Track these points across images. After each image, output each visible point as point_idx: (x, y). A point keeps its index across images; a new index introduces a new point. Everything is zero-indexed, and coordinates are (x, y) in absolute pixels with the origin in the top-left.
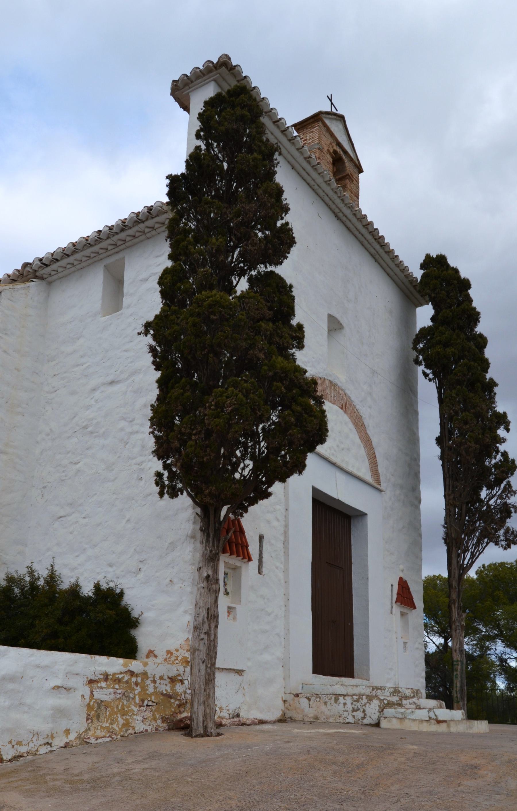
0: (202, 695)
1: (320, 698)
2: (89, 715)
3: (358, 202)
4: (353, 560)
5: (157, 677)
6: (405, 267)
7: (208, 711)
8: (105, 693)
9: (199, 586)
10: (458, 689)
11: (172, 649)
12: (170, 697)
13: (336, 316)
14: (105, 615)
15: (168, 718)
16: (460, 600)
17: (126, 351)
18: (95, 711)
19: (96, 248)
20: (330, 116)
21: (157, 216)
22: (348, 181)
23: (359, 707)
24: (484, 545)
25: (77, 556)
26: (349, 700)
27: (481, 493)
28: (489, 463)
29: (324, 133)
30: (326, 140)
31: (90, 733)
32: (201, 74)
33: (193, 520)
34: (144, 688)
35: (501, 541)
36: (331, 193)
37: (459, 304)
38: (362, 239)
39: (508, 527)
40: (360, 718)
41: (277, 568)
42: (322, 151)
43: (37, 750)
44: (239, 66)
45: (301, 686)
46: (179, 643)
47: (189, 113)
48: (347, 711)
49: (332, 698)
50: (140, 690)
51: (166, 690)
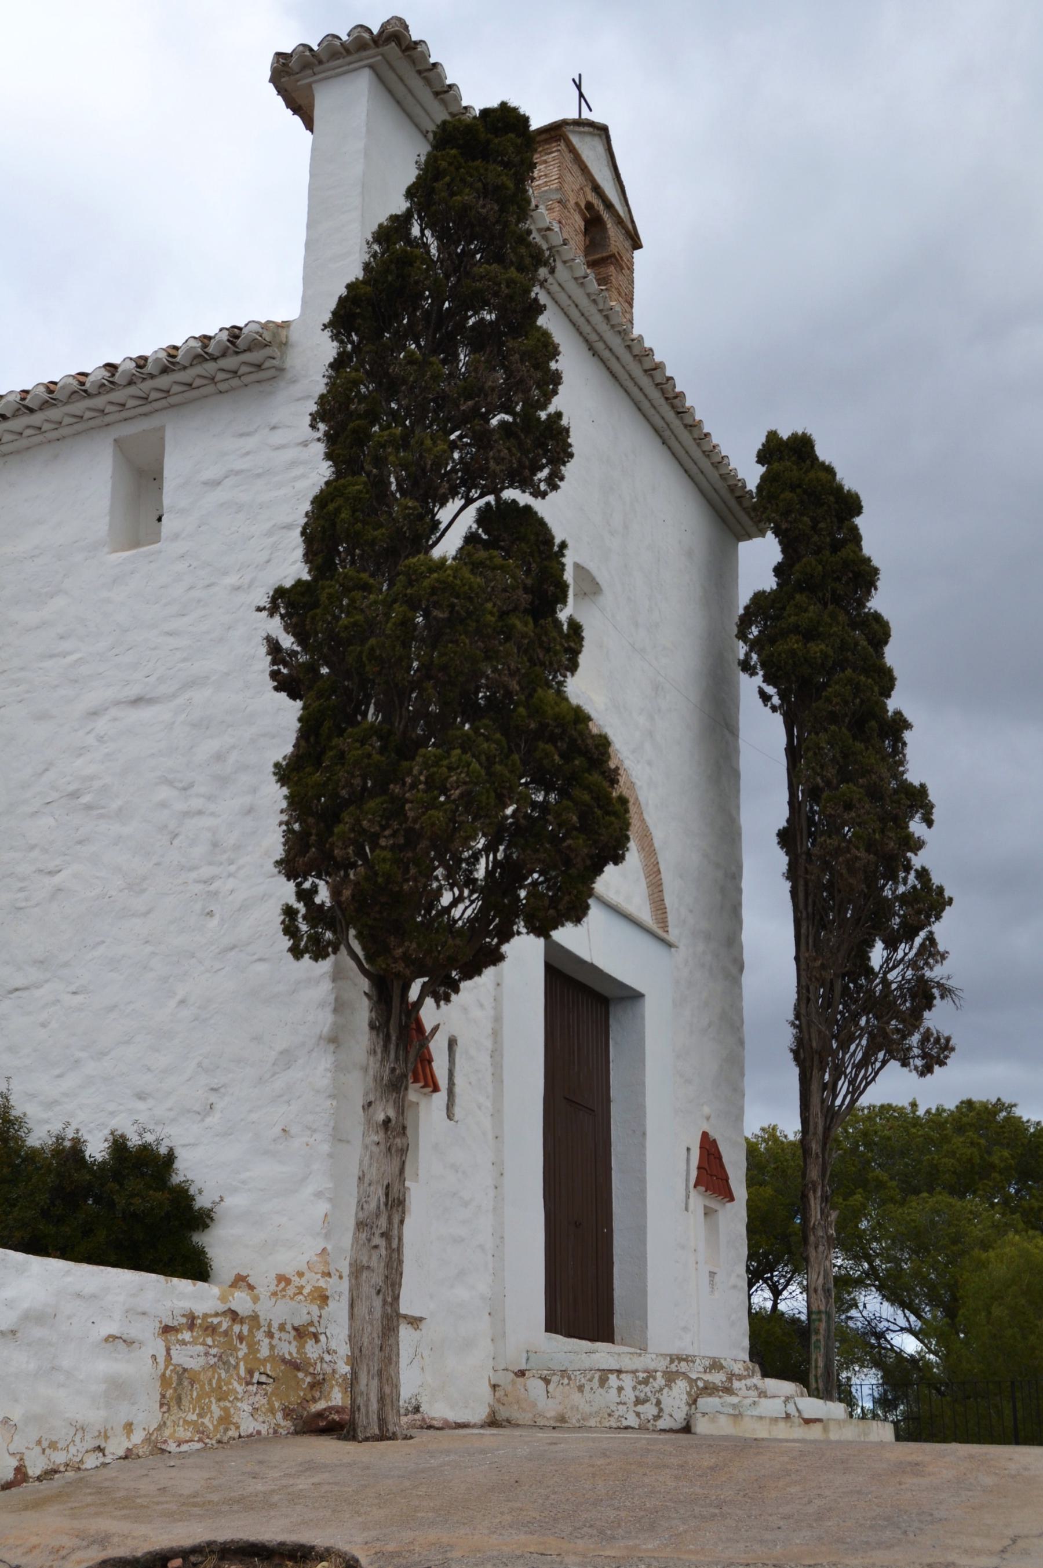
0: (376, 1358)
1: (569, 1378)
2: (163, 1396)
3: (632, 314)
4: (613, 1093)
5: (275, 1325)
6: (723, 458)
7: (387, 1390)
8: (190, 1353)
9: (368, 1141)
10: (820, 1371)
11: (289, 1271)
12: (297, 1367)
13: (588, 568)
14: (148, 1202)
15: (293, 1410)
16: (826, 1182)
17: (170, 634)
18: (176, 1387)
19: (99, 402)
20: (582, 129)
21: (249, 350)
22: (612, 268)
23: (649, 1394)
24: (878, 1065)
25: (58, 1076)
26: (628, 1381)
27: (871, 955)
28: (893, 893)
29: (570, 165)
30: (574, 181)
31: (167, 1432)
32: (343, 51)
33: (333, 1006)
34: (253, 1348)
35: (913, 1057)
36: (584, 302)
37: (836, 547)
38: (639, 396)
39: (928, 1029)
40: (650, 1417)
41: (480, 1108)
42: (565, 207)
43: (81, 1461)
44: (424, 42)
45: (525, 1355)
46: (306, 1258)
47: (309, 125)
48: (625, 1404)
49: (593, 1377)
50: (246, 1350)
51: (290, 1354)
